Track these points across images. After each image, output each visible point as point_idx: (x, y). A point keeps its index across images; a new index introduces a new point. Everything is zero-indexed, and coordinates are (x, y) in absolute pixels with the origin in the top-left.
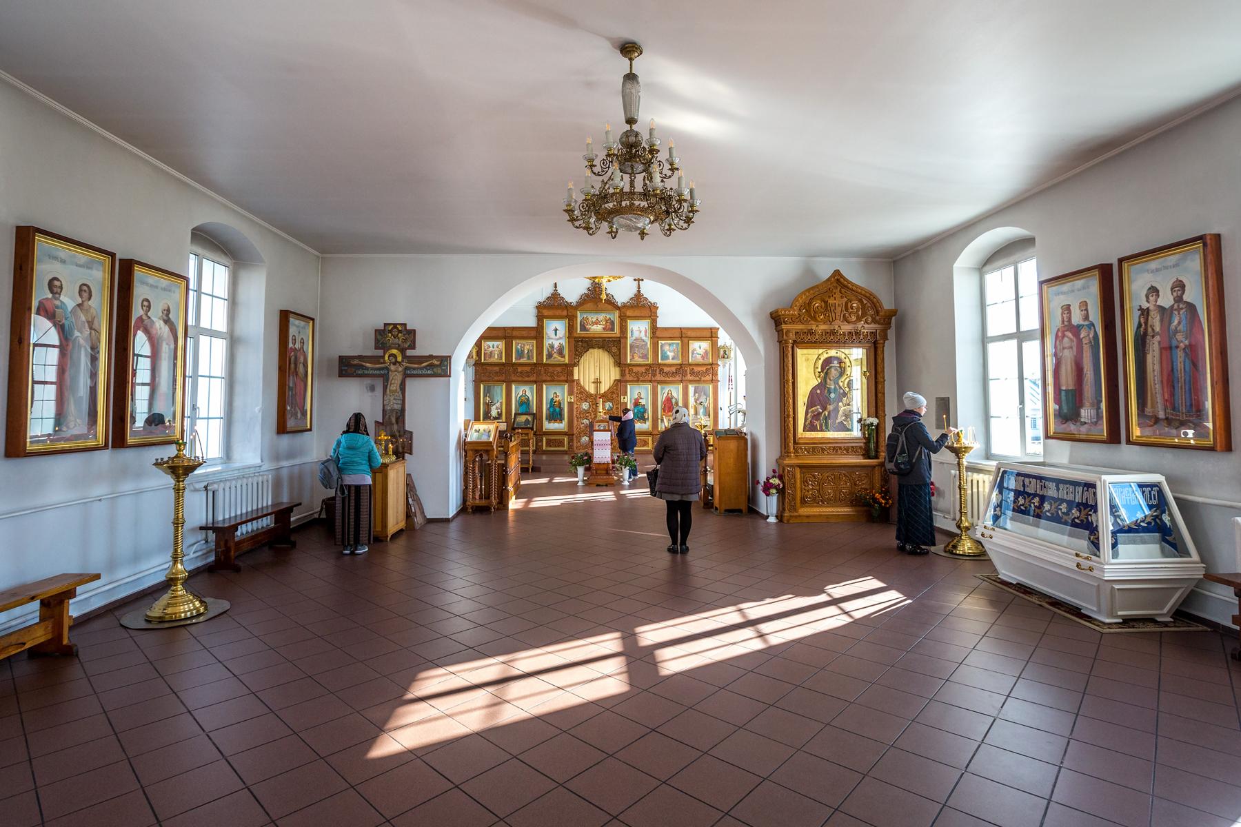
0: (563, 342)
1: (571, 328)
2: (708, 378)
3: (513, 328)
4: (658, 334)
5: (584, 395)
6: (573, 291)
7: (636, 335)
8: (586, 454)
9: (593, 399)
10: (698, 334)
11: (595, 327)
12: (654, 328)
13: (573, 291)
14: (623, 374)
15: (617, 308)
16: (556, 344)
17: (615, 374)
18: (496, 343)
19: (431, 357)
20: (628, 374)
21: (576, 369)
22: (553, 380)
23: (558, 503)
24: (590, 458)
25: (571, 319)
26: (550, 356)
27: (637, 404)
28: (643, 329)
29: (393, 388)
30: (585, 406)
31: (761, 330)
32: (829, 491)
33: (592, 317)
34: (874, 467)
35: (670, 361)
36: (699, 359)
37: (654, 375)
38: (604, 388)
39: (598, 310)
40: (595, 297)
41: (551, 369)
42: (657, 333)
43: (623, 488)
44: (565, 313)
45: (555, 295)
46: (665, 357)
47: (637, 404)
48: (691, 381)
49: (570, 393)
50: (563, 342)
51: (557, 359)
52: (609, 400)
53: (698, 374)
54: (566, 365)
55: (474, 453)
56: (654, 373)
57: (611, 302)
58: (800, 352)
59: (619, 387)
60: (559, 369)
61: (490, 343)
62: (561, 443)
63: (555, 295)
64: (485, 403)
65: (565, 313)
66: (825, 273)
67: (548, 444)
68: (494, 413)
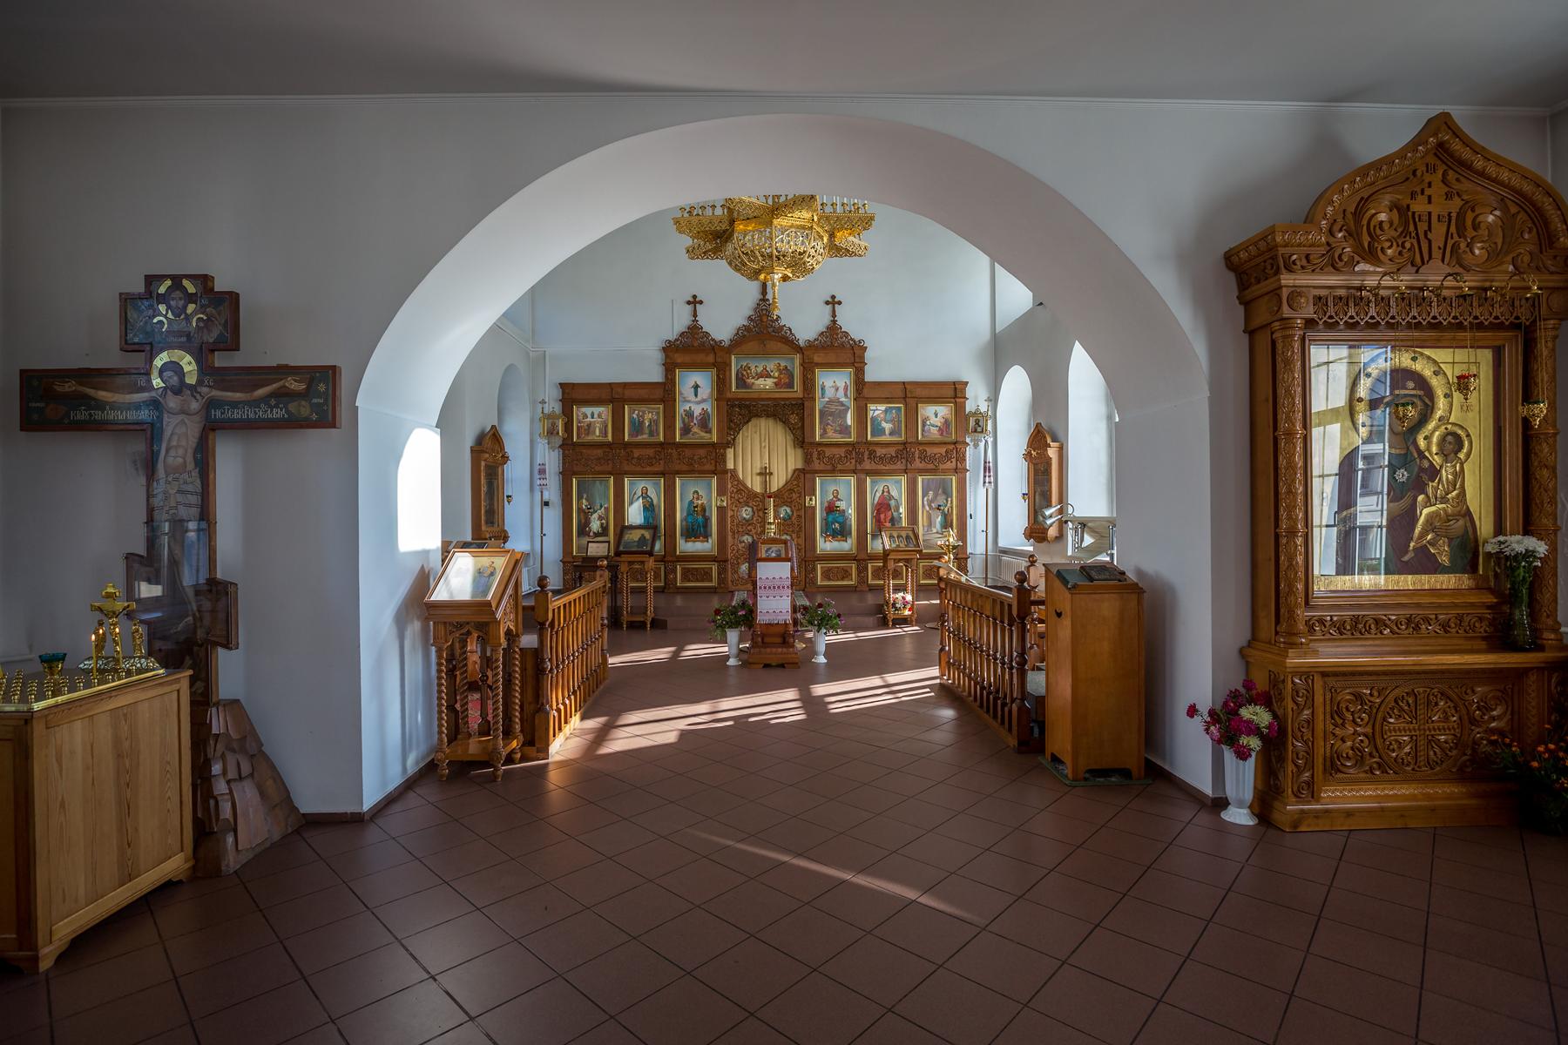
0: (707, 406)
1: (721, 384)
2: (951, 465)
3: (625, 385)
4: (866, 392)
5: (744, 495)
6: (722, 324)
7: (830, 393)
8: (744, 604)
9: (758, 501)
10: (933, 393)
11: (761, 381)
12: (860, 383)
13: (722, 324)
14: (807, 459)
15: (798, 349)
16: (697, 410)
17: (794, 460)
18: (597, 410)
19: (284, 370)
20: (818, 459)
21: (730, 453)
22: (692, 471)
23: (666, 735)
24: (751, 612)
25: (721, 369)
26: (686, 430)
27: (831, 509)
28: (841, 385)
29: (175, 459)
30: (746, 513)
31: (1200, 301)
32: (1400, 736)
33: (757, 366)
34: (1519, 674)
35: (886, 438)
36: (934, 433)
37: (860, 461)
38: (777, 482)
39: (766, 354)
40: (763, 330)
41: (688, 452)
42: (864, 392)
43: (814, 676)
44: (711, 359)
45: (694, 330)
46: (878, 431)
47: (831, 509)
48: (922, 471)
49: (721, 491)
50: (707, 406)
51: (698, 435)
52: (785, 503)
53: (932, 458)
54: (713, 445)
55: (451, 631)
56: (861, 457)
57: (787, 341)
58: (1317, 354)
59: (801, 481)
60: (702, 452)
61: (588, 410)
62: (706, 575)
63: (694, 330)
64: (580, 510)
65: (711, 359)
66: (1383, 130)
67: (685, 578)
68: (595, 525)
